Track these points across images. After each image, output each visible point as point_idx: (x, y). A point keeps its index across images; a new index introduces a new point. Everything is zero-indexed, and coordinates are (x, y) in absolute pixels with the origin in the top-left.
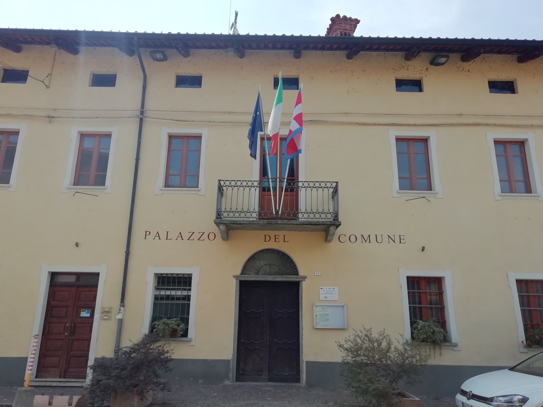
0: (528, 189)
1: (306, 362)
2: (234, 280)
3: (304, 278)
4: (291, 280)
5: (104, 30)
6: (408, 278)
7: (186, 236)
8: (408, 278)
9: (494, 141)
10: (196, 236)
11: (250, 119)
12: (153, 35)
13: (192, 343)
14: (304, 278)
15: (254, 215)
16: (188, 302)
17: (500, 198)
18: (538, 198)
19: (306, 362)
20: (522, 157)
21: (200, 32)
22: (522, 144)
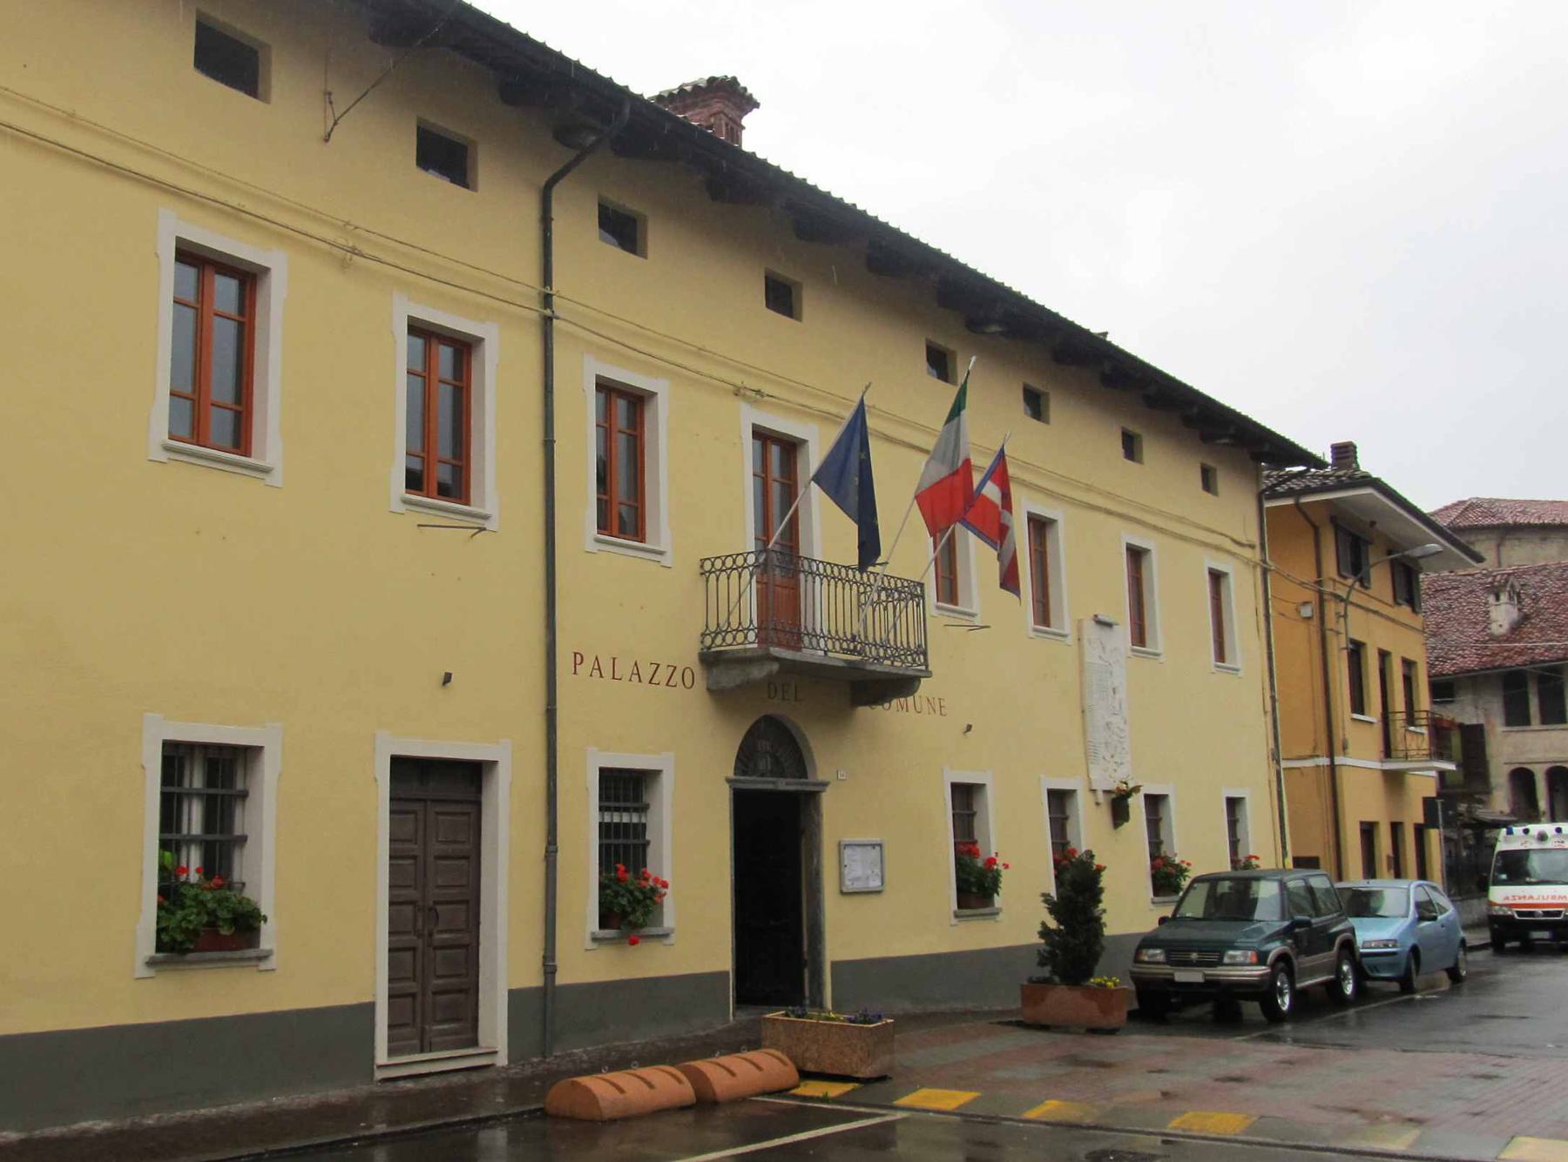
0: (241, 441)
1: (834, 964)
2: (727, 786)
3: (825, 784)
4: (760, 786)
5: (514, 26)
6: (602, 770)
7: (646, 673)
8: (602, 770)
9: (178, 250)
10: (663, 675)
11: (848, 414)
12: (542, 48)
13: (271, 963)
14: (825, 784)
15: (752, 636)
16: (168, 836)
17: (164, 457)
18: (658, 558)
19: (834, 964)
20: (241, 325)
21: (537, 35)
22: (249, 278)
